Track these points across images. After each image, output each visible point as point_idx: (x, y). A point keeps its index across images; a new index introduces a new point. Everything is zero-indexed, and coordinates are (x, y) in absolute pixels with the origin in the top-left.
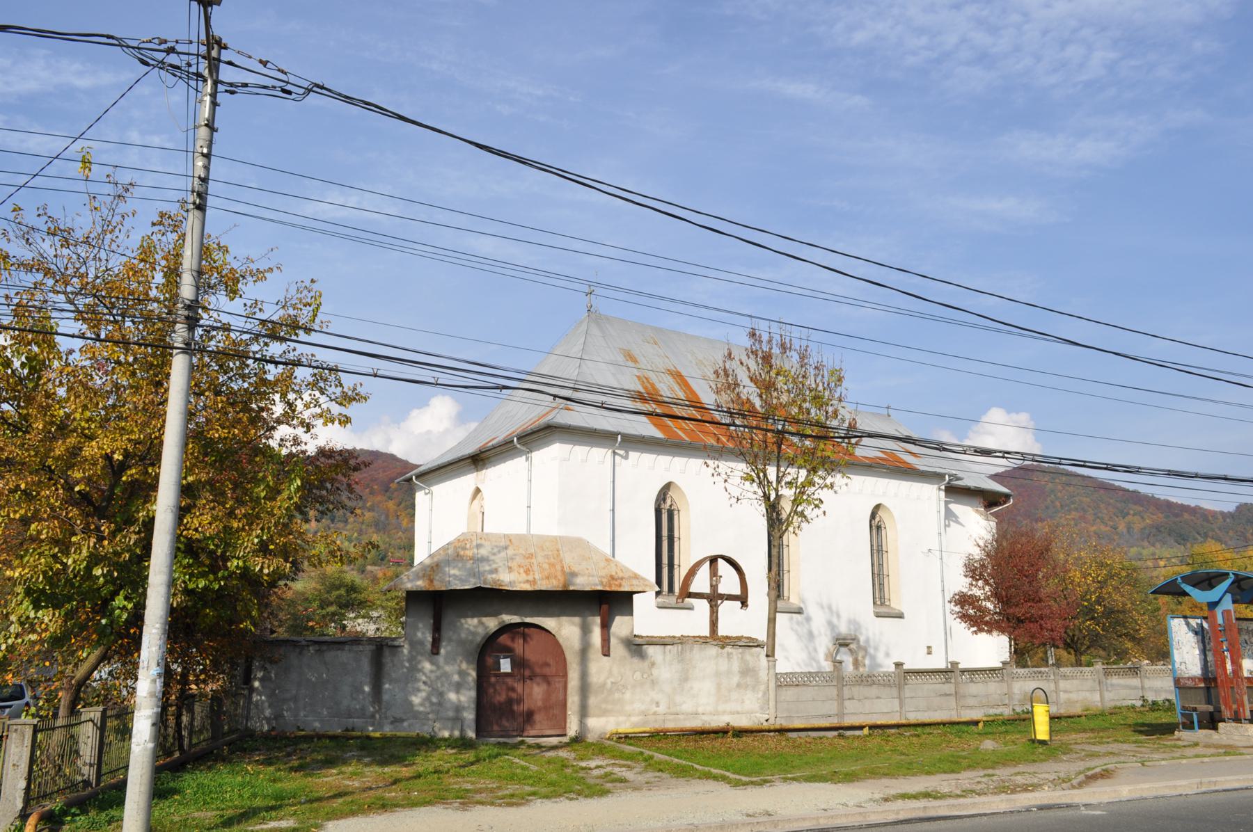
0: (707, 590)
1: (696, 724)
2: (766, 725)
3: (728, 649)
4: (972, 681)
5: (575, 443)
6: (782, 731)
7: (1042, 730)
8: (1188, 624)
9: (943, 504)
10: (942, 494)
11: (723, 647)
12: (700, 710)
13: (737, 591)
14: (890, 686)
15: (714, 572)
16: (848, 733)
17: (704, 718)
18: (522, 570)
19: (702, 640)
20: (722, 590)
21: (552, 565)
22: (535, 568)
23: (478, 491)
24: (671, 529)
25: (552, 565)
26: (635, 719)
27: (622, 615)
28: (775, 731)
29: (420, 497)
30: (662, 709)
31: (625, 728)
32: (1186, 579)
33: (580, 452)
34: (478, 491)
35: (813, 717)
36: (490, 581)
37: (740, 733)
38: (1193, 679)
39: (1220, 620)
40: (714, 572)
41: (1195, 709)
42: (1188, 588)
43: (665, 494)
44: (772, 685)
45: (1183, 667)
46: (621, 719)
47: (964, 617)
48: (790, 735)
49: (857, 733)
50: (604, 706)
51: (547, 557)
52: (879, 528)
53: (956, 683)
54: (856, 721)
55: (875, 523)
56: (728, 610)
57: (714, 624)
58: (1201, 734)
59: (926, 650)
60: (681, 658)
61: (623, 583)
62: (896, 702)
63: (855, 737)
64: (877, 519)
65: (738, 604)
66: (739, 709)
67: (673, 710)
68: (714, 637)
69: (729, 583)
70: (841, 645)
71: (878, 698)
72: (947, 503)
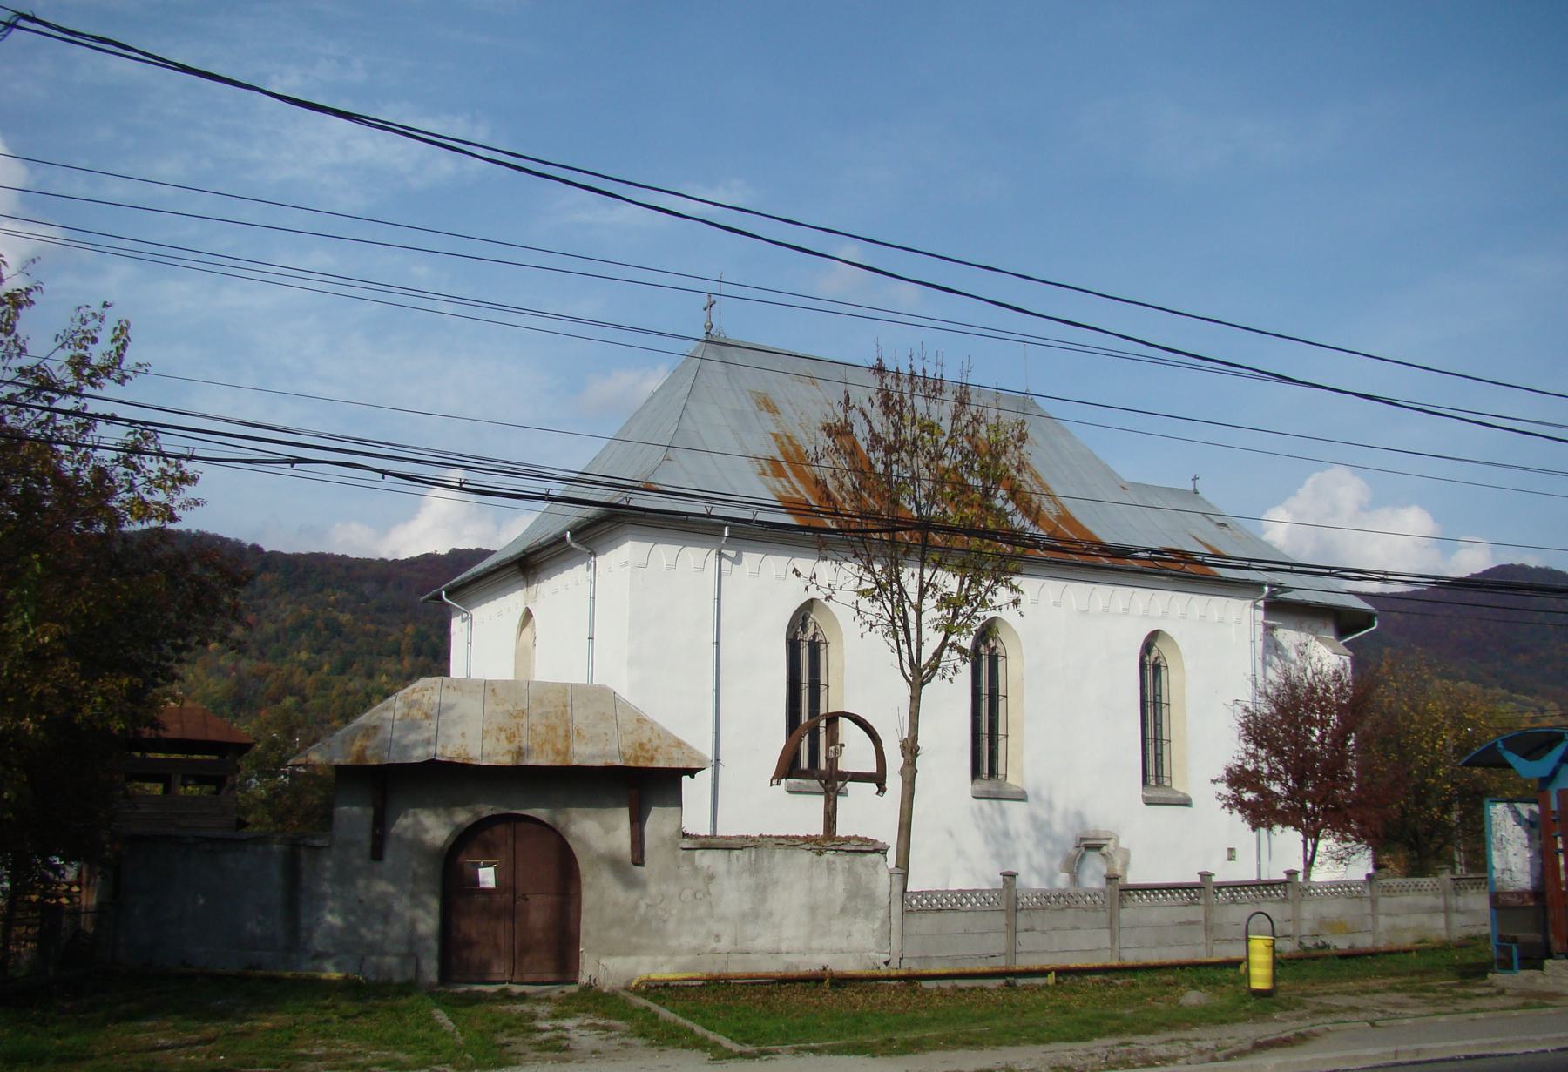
1: (773, 967)
2: (884, 970)
3: (829, 855)
4: (1234, 901)
6: (911, 979)
7: (1260, 977)
8: (1516, 813)
9: (1260, 629)
10: (1260, 615)
11: (820, 854)
12: (784, 947)
13: (872, 768)
14: (1095, 910)
16: (1021, 982)
17: (789, 958)
18: (503, 736)
20: (844, 765)
22: (524, 732)
23: (528, 615)
26: (680, 960)
27: (664, 805)
28: (899, 978)
29: (457, 626)
30: (725, 944)
32: (1510, 744)
34: (528, 615)
35: (963, 957)
37: (841, 981)
38: (1520, 894)
39: (1554, 806)
41: (1514, 940)
42: (1511, 758)
43: (805, 619)
44: (896, 910)
45: (1506, 877)
46: (661, 959)
47: (1238, 803)
48: (925, 984)
49: (1039, 981)
50: (634, 940)
51: (546, 715)
52: (1157, 668)
53: (1207, 905)
54: (1034, 962)
55: (1150, 660)
56: (857, 797)
58: (1520, 978)
60: (754, 869)
61: (657, 756)
62: (1106, 934)
63: (1031, 989)
64: (1154, 654)
65: (873, 787)
66: (844, 944)
67: (739, 947)
68: (828, 841)
70: (1088, 848)
71: (1075, 928)
72: (1269, 629)
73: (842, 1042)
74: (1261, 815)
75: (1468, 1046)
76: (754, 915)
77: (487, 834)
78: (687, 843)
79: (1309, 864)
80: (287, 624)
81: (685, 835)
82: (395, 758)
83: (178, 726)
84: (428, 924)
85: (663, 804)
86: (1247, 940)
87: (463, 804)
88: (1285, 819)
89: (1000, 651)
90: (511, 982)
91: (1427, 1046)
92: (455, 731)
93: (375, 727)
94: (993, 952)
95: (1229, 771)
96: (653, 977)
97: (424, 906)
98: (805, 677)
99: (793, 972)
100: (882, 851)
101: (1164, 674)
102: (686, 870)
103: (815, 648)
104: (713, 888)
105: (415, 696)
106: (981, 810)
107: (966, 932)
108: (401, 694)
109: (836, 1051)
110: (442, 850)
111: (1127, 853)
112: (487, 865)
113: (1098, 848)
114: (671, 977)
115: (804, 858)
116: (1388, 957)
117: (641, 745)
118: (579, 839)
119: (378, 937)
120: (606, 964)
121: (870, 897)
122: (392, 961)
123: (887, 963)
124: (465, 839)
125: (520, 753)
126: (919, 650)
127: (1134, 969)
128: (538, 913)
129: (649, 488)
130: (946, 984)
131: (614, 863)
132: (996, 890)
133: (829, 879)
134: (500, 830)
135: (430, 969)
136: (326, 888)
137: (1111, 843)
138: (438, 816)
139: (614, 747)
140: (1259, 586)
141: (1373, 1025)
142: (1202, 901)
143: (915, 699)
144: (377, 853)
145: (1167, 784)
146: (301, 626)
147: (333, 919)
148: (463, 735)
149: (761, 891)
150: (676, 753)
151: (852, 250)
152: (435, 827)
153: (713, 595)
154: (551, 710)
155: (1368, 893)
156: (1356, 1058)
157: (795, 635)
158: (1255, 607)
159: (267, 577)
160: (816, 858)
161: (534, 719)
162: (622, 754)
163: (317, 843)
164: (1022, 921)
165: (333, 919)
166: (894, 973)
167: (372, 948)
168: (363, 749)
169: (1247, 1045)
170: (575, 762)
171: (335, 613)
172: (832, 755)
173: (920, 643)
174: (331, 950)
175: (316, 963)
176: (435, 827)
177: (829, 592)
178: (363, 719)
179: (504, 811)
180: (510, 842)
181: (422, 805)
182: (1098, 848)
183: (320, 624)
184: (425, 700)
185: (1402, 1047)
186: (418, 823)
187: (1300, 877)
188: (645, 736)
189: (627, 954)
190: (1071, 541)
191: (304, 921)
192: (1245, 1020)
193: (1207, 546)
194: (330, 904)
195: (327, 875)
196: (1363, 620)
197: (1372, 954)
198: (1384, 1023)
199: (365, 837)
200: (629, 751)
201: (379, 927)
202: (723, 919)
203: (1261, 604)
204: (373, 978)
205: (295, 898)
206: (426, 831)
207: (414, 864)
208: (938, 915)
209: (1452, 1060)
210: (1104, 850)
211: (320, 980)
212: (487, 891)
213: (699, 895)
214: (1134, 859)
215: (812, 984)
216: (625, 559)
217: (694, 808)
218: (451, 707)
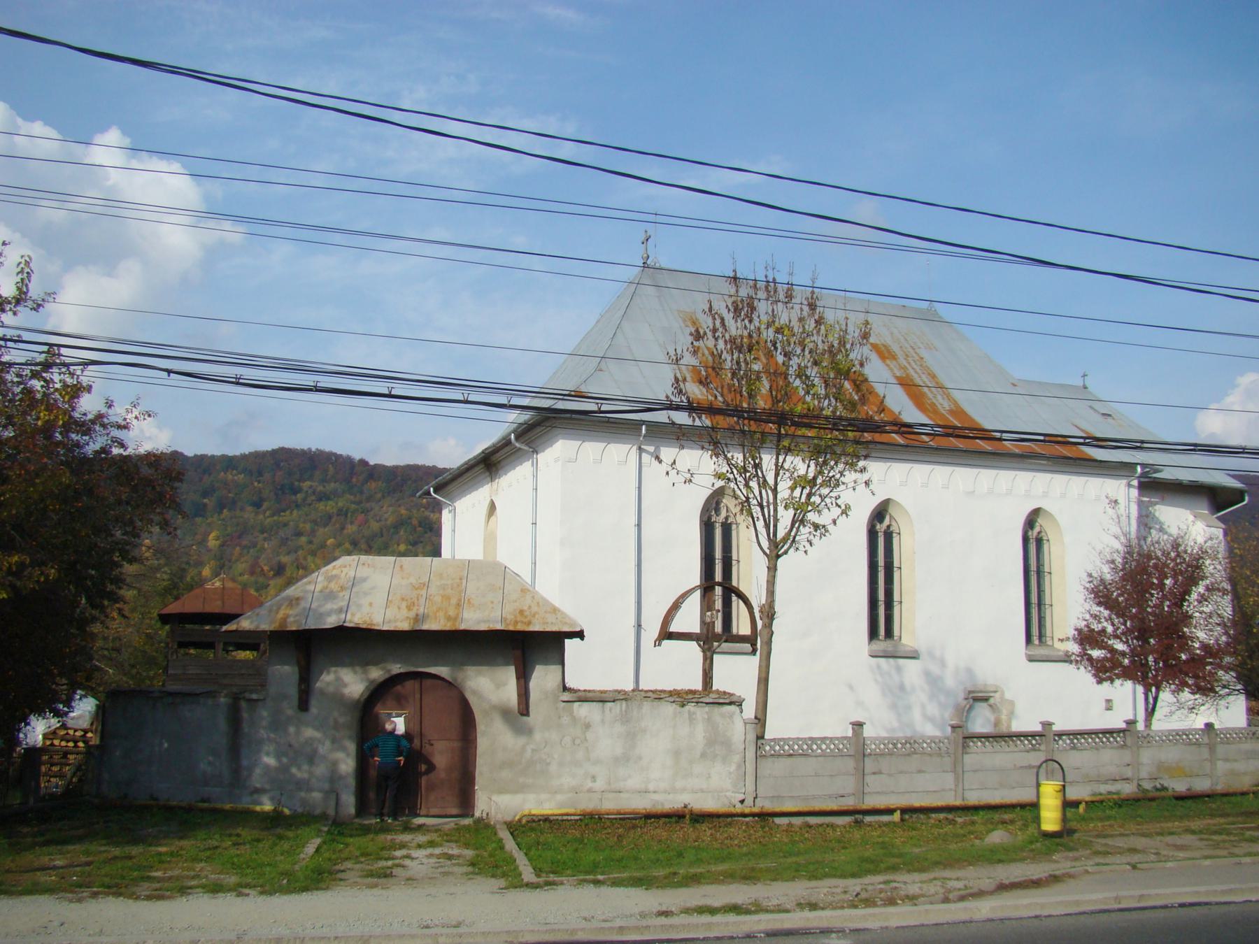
0: (696, 628)
2: (739, 808)
4: (1074, 748)
7: (1050, 819)
10: (1134, 493)
11: (683, 706)
12: (651, 787)
14: (940, 755)
16: (868, 819)
17: (655, 797)
18: (404, 604)
19: (681, 698)
21: (447, 598)
22: (422, 601)
23: (492, 507)
25: (447, 598)
27: (546, 663)
28: (753, 815)
30: (600, 784)
34: (492, 507)
35: (814, 797)
36: (356, 618)
37: (700, 818)
43: (718, 503)
44: (751, 754)
46: (543, 796)
48: (778, 820)
49: (885, 818)
50: (521, 780)
52: (1039, 542)
55: (1033, 534)
59: (1104, 704)
60: (625, 719)
61: (534, 621)
64: (1037, 529)
68: (707, 695)
70: (976, 699)
71: (920, 771)
73: (625, 875)
74: (1105, 671)
75: (1197, 893)
76: (625, 759)
77: (399, 688)
78: (566, 696)
79: (1150, 712)
80: (389, 522)
82: (312, 624)
83: (219, 603)
84: (347, 764)
85: (546, 662)
86: (1038, 785)
87: (375, 663)
88: (1127, 674)
89: (894, 528)
91: (1153, 892)
92: (365, 601)
93: (298, 599)
94: (841, 792)
95: (1079, 631)
96: (534, 812)
97: (344, 749)
98: (881, 562)
99: (659, 809)
100: (739, 703)
101: (1046, 547)
102: (566, 720)
104: (589, 735)
105: (334, 572)
106: (879, 667)
107: (816, 775)
108: (324, 570)
109: (616, 883)
110: (358, 700)
111: (1012, 703)
112: (399, 716)
113: (986, 699)
114: (550, 812)
115: (669, 709)
116: (1225, 799)
117: (521, 612)
118: (474, 692)
119: (306, 776)
120: (497, 801)
121: (727, 744)
122: (317, 795)
123: (742, 802)
124: (379, 692)
125: (417, 619)
126: (775, 526)
127: (976, 809)
129: (579, 395)
130: (797, 821)
131: (505, 713)
132: (845, 738)
133: (694, 726)
134: (409, 685)
135: (349, 802)
136: (263, 733)
137: (997, 695)
138: (355, 673)
140: (1130, 467)
141: (1134, 867)
142: (1043, 747)
143: (772, 569)
144: (304, 705)
145: (1049, 643)
146: (397, 526)
147: (270, 761)
148: (371, 604)
149: (631, 738)
150: (551, 618)
151: (866, 210)
152: (352, 682)
153: (635, 484)
155: (1206, 740)
156: (1077, 903)
157: (710, 518)
158: (1129, 485)
159: (373, 485)
160: (678, 708)
162: (503, 619)
163: (254, 696)
164: (869, 764)
165: (270, 761)
166: (747, 811)
167: (301, 785)
168: (285, 620)
169: (993, 887)
170: (463, 627)
171: (427, 513)
173: (776, 520)
174: (267, 787)
175: (255, 796)
176: (352, 682)
177: (688, 476)
178: (291, 591)
179: (412, 669)
180: (418, 696)
182: (986, 699)
183: (415, 522)
185: (1121, 893)
186: (338, 679)
187: (1140, 726)
189: (516, 792)
190: (955, 428)
191: (245, 763)
192: (1023, 860)
193: (1083, 431)
194: (266, 748)
195: (264, 723)
196: (1237, 496)
197: (1208, 796)
198: (1145, 866)
199: (293, 691)
200: (510, 617)
201: (305, 767)
203: (1135, 483)
204: (300, 810)
205: (237, 742)
206: (345, 685)
207: (336, 714)
208: (789, 761)
209: (1165, 907)
210: (992, 701)
213: (577, 742)
214: (1020, 708)
215: (673, 820)
216: (560, 454)
217: (584, 666)
218: (364, 580)
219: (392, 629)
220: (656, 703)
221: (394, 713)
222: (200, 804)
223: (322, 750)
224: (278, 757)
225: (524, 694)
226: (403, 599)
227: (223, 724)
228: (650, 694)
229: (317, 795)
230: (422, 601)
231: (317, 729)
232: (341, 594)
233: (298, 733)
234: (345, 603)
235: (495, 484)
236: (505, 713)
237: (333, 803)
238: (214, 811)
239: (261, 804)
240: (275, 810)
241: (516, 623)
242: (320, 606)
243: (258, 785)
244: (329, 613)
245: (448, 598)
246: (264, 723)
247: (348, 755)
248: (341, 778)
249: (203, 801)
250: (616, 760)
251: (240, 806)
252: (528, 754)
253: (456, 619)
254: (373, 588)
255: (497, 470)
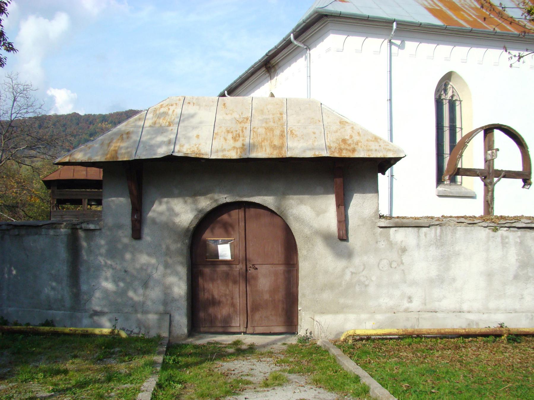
3: (503, 231)
5: (349, 33)
11: (495, 230)
12: (465, 307)
13: (518, 167)
15: (489, 145)
17: (471, 317)
18: (230, 136)
19: (471, 222)
20: (499, 165)
21: (270, 130)
22: (247, 133)
24: (453, 119)
26: (379, 317)
27: (364, 191)
30: (416, 304)
31: (368, 327)
33: (354, 41)
36: (184, 149)
40: (489, 145)
43: (446, 85)
46: (364, 316)
50: (342, 301)
51: (266, 121)
57: (489, 204)
60: (440, 243)
61: (358, 148)
66: (517, 306)
67: (429, 307)
69: (508, 157)
76: (440, 280)
77: (225, 217)
78: (383, 223)
81: (381, 217)
82: (143, 155)
84: (180, 289)
85: (364, 191)
87: (204, 194)
90: (245, 333)
93: (128, 133)
96: (358, 332)
97: (177, 274)
99: (474, 328)
102: (382, 244)
103: (452, 105)
104: (406, 259)
110: (187, 230)
117: (344, 141)
118: (297, 219)
120: (319, 321)
124: (207, 220)
128: (266, 279)
131: (327, 238)
134: (236, 214)
138: (185, 202)
139: (321, 142)
147: (109, 285)
148: (198, 136)
149: (446, 260)
150: (374, 146)
152: (181, 211)
154: (271, 116)
157: (440, 96)
160: (492, 234)
161: (256, 123)
162: (329, 148)
163: (92, 227)
165: (109, 285)
167: (136, 307)
168: (116, 152)
170: (289, 155)
172: (489, 157)
174: (106, 310)
175: (96, 318)
176: (181, 211)
180: (242, 224)
181: (172, 195)
184: (170, 112)
186: (171, 210)
188: (347, 133)
189: (337, 312)
191: (84, 288)
199: (127, 221)
201: (141, 291)
202: (414, 283)
206: (177, 215)
207: (169, 241)
211: (95, 335)
212: (225, 262)
213: (394, 265)
215: (491, 338)
216: (332, 44)
219: (220, 157)
220: (469, 228)
221: (220, 240)
222: (42, 328)
223: (157, 275)
224: (115, 281)
225: (343, 221)
226: (228, 132)
227: (63, 253)
228: (462, 220)
229: (152, 317)
230: (247, 133)
231: (149, 255)
232: (170, 128)
233: (133, 260)
234: (173, 136)
235: (274, 81)
236: (327, 238)
237: (167, 324)
238: (57, 334)
239: (100, 326)
240: (112, 332)
241: (341, 150)
242: (151, 139)
243: (98, 308)
244: (160, 145)
245: (271, 130)
246: (103, 251)
247: (180, 279)
248: (174, 300)
249: (48, 323)
250: (431, 281)
251: (79, 329)
252: (348, 277)
253: (281, 147)
254: (201, 123)
255: (275, 71)
